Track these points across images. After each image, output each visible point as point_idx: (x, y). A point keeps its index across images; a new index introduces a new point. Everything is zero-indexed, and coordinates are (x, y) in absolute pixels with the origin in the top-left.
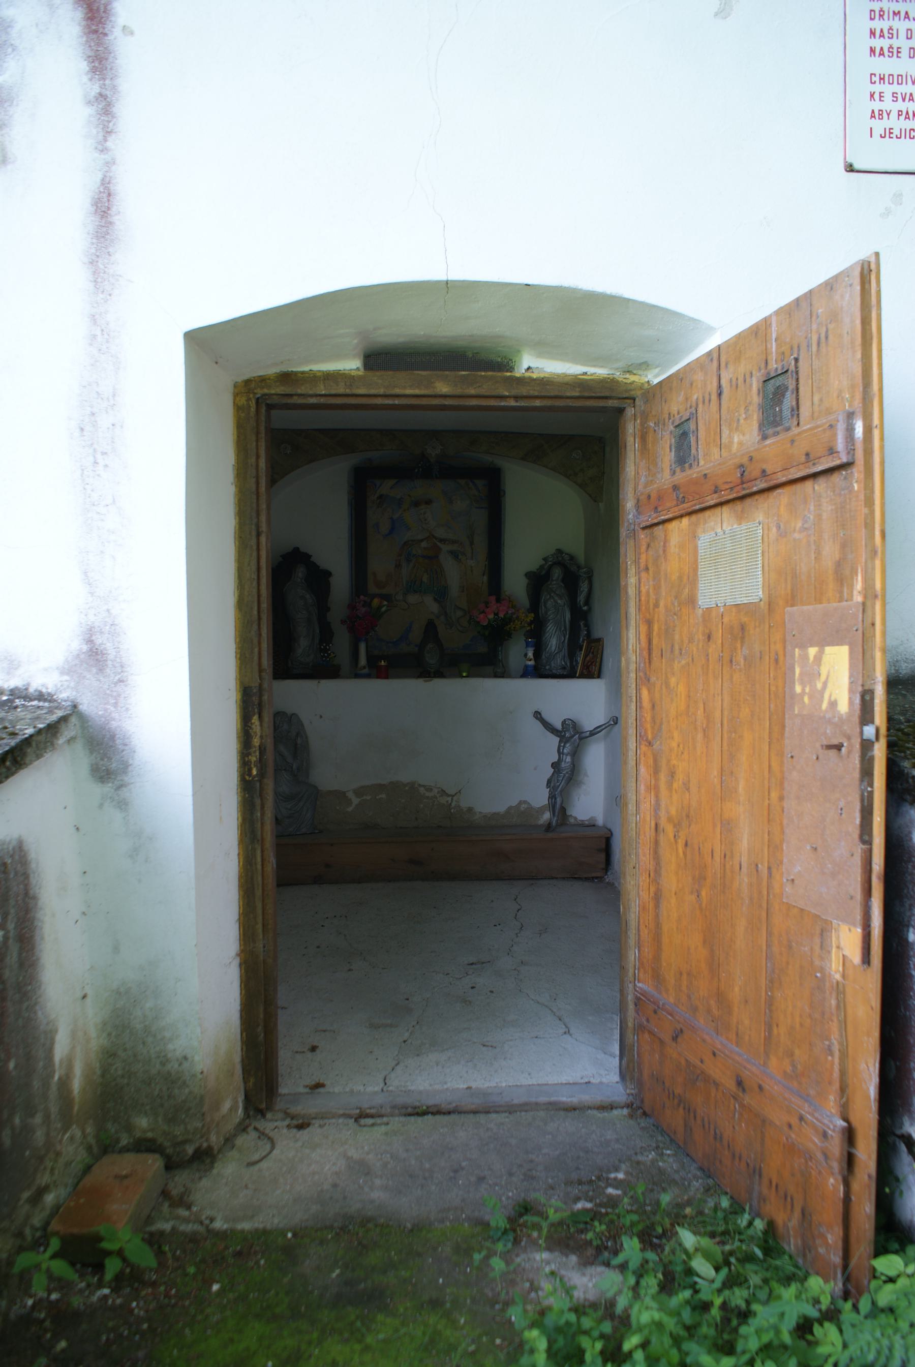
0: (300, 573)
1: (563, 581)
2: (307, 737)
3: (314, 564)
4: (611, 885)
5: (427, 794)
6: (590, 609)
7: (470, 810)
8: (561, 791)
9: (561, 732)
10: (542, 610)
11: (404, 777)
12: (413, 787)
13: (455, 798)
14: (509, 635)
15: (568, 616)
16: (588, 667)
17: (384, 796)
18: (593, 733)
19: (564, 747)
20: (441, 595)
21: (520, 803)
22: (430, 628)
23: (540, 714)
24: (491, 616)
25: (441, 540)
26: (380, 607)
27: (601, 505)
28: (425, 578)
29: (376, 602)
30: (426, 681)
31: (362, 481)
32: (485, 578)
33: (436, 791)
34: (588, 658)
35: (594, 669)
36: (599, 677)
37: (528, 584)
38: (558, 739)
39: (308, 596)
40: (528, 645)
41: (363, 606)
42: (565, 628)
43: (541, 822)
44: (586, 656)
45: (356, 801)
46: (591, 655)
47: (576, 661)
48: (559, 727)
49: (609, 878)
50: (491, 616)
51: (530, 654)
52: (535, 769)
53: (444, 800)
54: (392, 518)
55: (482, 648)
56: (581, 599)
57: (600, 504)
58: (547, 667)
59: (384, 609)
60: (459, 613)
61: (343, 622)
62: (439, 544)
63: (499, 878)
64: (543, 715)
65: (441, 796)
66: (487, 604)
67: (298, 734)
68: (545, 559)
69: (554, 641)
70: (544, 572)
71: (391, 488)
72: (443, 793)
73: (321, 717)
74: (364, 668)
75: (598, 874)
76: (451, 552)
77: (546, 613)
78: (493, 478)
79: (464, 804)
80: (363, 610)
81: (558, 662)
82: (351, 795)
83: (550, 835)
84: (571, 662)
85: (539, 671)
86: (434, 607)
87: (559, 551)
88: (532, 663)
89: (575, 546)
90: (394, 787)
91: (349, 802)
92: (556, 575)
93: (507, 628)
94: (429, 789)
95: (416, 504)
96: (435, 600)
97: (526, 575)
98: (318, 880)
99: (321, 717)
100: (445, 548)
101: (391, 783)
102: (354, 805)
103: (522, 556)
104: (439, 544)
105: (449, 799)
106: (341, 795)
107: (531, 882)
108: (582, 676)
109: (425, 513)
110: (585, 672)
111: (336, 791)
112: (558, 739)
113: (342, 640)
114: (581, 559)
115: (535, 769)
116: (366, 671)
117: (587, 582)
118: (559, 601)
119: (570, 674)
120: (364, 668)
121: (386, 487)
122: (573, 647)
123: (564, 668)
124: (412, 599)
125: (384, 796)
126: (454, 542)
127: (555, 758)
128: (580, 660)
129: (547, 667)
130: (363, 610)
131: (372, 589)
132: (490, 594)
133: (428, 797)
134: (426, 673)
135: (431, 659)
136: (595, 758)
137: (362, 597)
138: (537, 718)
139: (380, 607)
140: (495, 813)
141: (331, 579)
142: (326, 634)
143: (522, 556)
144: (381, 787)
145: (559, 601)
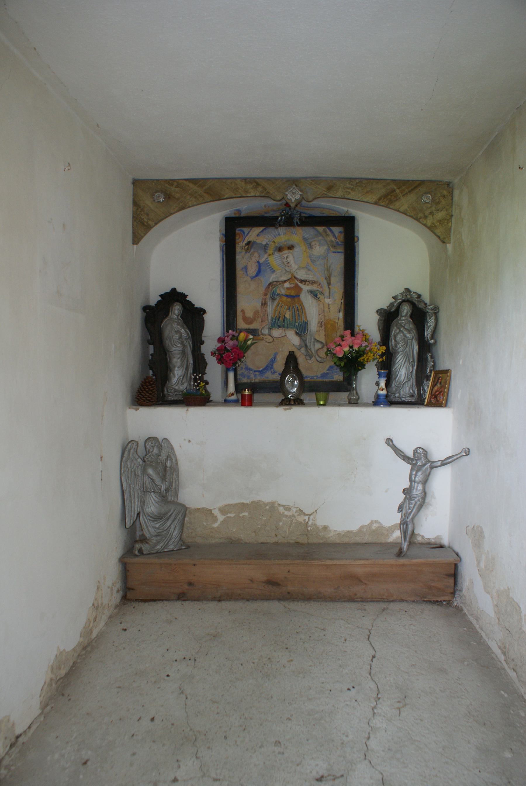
0: (177, 309)
1: (411, 317)
2: (176, 460)
3: (189, 302)
4: (459, 609)
5: (286, 513)
6: (436, 342)
7: (325, 528)
8: (413, 519)
9: (412, 460)
10: (392, 343)
11: (266, 497)
12: (273, 506)
13: (312, 517)
14: (363, 366)
15: (416, 348)
16: (436, 397)
17: (246, 514)
18: (444, 463)
19: (416, 475)
20: (302, 330)
21: (372, 522)
22: (292, 361)
23: (392, 441)
24: (346, 349)
25: (302, 281)
26: (246, 340)
27: (449, 246)
28: (288, 315)
29: (242, 336)
30: (285, 409)
31: (233, 226)
32: (341, 315)
33: (294, 510)
34: (436, 388)
35: (441, 398)
36: (446, 406)
37: (379, 320)
38: (410, 466)
39: (183, 331)
40: (379, 375)
41: (231, 339)
42: (413, 358)
43: (391, 540)
44: (434, 385)
45: (221, 518)
46: (438, 385)
47: (424, 389)
48: (411, 455)
49: (456, 602)
50: (346, 349)
51: (383, 384)
52: (386, 491)
53: (301, 519)
54: (258, 262)
55: (338, 376)
56: (428, 333)
57: (448, 245)
58: (397, 395)
59: (249, 342)
60: (318, 346)
61: (213, 354)
62: (300, 284)
63: (351, 600)
64: (395, 442)
65: (299, 515)
66: (342, 337)
67: (168, 457)
68: (395, 298)
69: (403, 370)
70: (393, 310)
71: (258, 235)
72: (301, 512)
73: (189, 441)
74: (233, 394)
75: (447, 598)
76: (311, 292)
77: (396, 346)
78: (348, 223)
79: (320, 523)
80: (231, 343)
81: (407, 390)
82: (216, 512)
83: (402, 561)
84: (419, 391)
85: (389, 401)
86: (296, 340)
87: (408, 290)
88: (384, 392)
89: (421, 287)
90: (256, 506)
91: (215, 519)
92: (405, 311)
93: (361, 359)
94: (288, 509)
95: (280, 249)
96: (297, 333)
97: (377, 311)
98: (182, 597)
99: (189, 441)
100: (305, 288)
101: (253, 502)
102: (219, 522)
103: (373, 297)
104: (300, 284)
105: (306, 518)
106: (208, 512)
107: (383, 605)
108: (430, 404)
109: (287, 257)
110: (433, 401)
111: (203, 508)
112: (410, 466)
113: (214, 371)
114: (426, 297)
115: (386, 491)
116: (234, 397)
117: (433, 317)
118: (408, 335)
119: (418, 402)
120: (233, 394)
121: (253, 234)
122: (421, 376)
123: (412, 396)
124: (277, 333)
125: (246, 514)
126: (313, 283)
127: (407, 485)
128: (428, 390)
129: (397, 395)
130: (231, 343)
131: (241, 324)
132: (346, 329)
133: (286, 516)
134: (287, 402)
135: (293, 387)
136: (442, 482)
137: (230, 331)
138: (389, 445)
139: (246, 340)
140: (348, 532)
141: (205, 316)
142: (199, 365)
143: (373, 297)
144: (243, 506)
145: (408, 335)
